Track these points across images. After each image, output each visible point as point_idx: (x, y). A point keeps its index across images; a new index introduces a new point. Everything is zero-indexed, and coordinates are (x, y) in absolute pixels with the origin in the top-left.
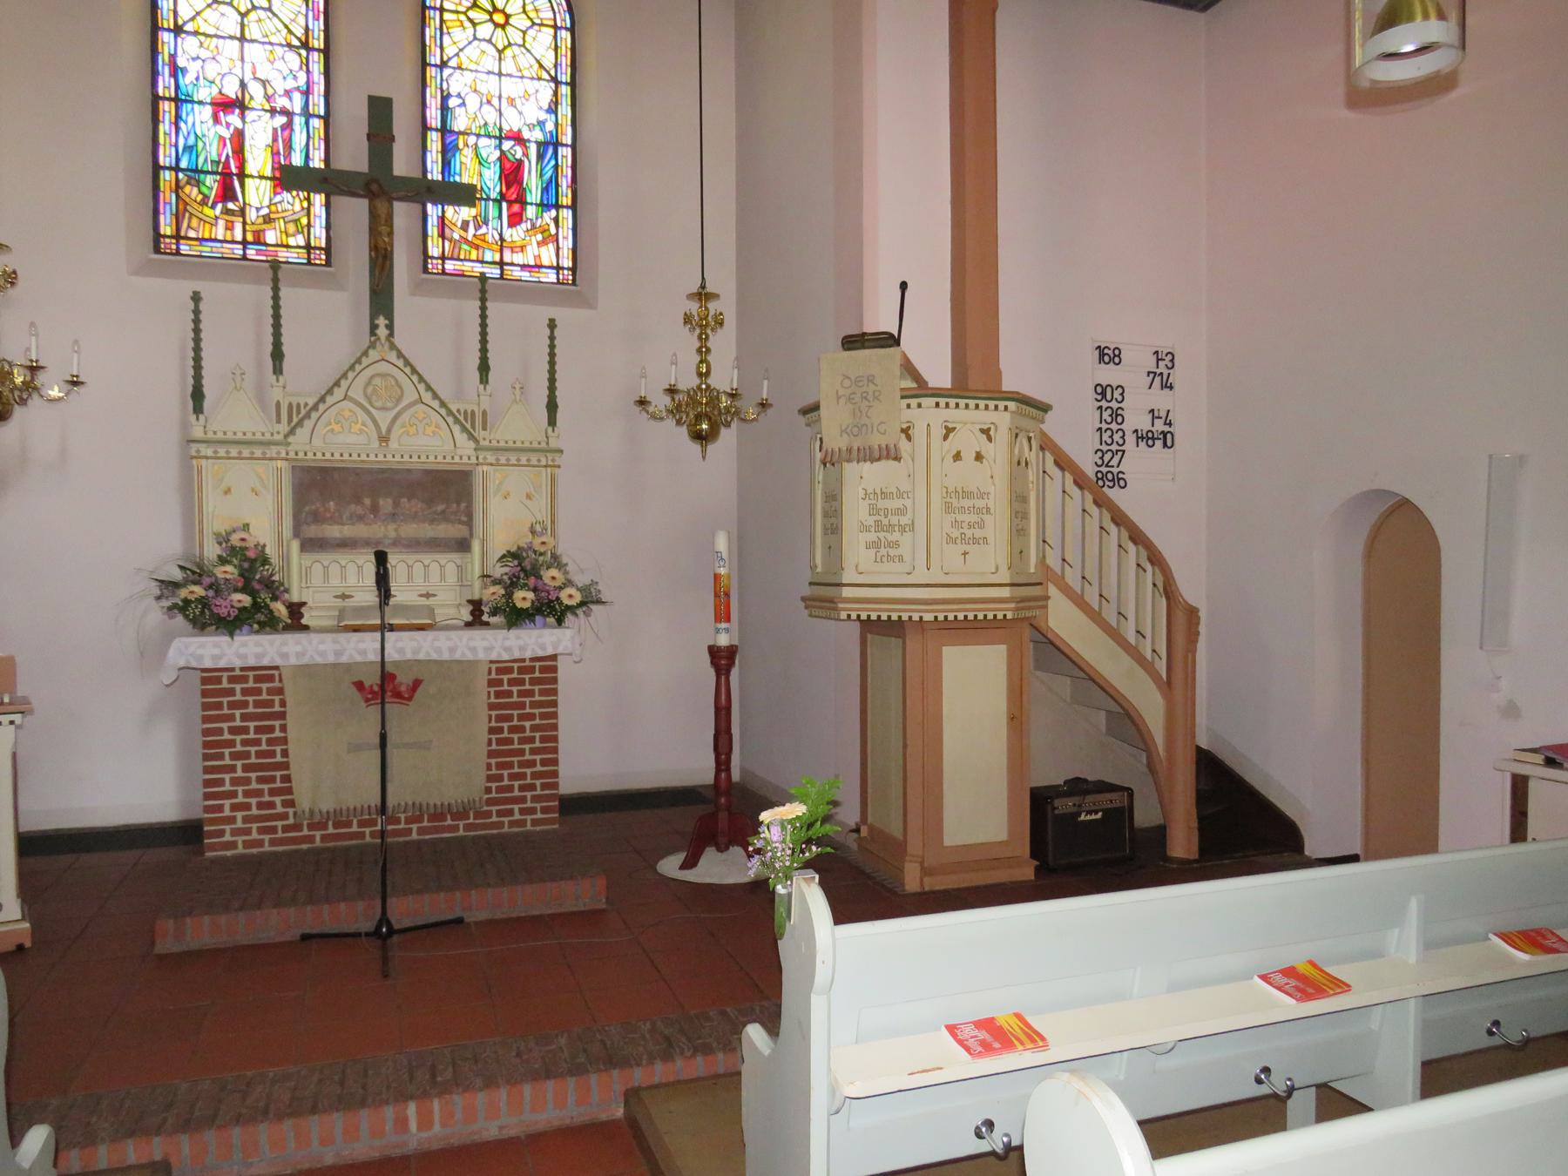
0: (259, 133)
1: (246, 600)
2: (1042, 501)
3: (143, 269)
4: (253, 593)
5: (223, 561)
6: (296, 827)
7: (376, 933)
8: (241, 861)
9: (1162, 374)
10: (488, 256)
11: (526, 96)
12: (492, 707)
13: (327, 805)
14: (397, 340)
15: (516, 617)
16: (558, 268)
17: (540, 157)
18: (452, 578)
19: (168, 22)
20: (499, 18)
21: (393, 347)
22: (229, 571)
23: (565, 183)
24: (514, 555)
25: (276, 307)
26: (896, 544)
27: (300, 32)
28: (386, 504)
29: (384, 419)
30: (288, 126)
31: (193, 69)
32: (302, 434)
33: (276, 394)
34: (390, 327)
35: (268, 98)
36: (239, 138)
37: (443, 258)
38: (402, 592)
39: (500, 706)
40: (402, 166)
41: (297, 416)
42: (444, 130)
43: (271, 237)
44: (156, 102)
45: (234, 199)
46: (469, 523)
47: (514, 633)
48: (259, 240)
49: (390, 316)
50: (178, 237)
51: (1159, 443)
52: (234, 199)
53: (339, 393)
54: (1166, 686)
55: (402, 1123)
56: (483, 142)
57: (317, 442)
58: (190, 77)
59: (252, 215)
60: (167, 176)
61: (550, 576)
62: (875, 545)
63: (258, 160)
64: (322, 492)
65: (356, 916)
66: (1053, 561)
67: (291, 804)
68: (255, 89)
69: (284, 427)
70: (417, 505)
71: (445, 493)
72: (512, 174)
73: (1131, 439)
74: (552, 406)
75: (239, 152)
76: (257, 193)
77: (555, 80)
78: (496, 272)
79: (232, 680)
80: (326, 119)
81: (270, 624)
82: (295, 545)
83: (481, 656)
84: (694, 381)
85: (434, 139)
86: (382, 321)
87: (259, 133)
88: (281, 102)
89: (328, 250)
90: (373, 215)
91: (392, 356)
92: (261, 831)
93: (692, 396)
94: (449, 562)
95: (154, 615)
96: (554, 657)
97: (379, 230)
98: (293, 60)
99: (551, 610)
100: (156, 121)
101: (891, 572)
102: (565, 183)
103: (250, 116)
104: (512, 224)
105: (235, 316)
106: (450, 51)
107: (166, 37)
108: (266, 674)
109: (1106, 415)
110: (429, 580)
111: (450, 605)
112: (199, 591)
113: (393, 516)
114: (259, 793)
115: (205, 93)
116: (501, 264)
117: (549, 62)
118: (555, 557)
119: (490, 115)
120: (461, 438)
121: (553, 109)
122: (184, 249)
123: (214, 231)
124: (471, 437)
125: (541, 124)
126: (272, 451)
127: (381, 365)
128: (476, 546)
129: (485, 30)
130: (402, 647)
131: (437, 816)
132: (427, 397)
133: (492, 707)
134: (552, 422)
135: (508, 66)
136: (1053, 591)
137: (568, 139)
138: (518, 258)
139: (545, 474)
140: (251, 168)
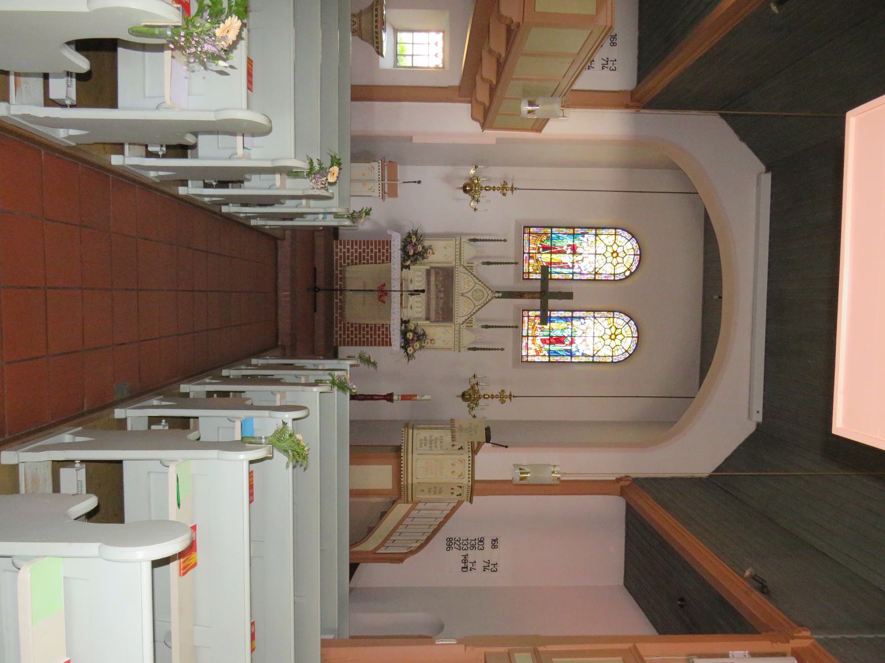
0: (566, 258)
1: (411, 253)
2: (439, 501)
3: (517, 223)
4: (413, 255)
5: (423, 247)
6: (341, 266)
7: (315, 287)
8: (332, 251)
9: (490, 567)
10: (530, 332)
11: (587, 345)
12: (375, 325)
13: (347, 275)
14: (494, 300)
15: (404, 334)
16: (527, 356)
17: (566, 350)
18: (416, 315)
19: (598, 232)
20: (613, 337)
21: (492, 298)
22: (420, 248)
23: (558, 359)
24: (424, 334)
25: (509, 263)
26: (425, 445)
27: (600, 272)
28: (442, 295)
29: (469, 295)
30: (569, 267)
31: (585, 239)
32: (463, 270)
33: (476, 263)
34: (499, 297)
35: (577, 262)
36: (564, 252)
37: (528, 316)
38: (413, 300)
39: (375, 328)
40: (552, 303)
41: (469, 269)
42: (572, 318)
43: (531, 261)
44: (575, 229)
45: (543, 250)
46: (435, 321)
47: (399, 332)
48: (530, 257)
49: (502, 297)
50: (530, 233)
51: (463, 565)
52: (543, 250)
53: (477, 281)
54: (374, 552)
55: (286, 291)
56: (570, 331)
57: (461, 274)
58: (581, 238)
59: (538, 256)
60: (549, 230)
61: (417, 345)
62: (425, 439)
63: (556, 258)
64: (445, 277)
65: (320, 283)
66: (420, 506)
67: (348, 265)
68: (580, 258)
69: (465, 265)
70: (441, 305)
71: (446, 314)
72: (559, 340)
73: (464, 553)
74: (475, 349)
75: (559, 252)
76: (545, 258)
77: (594, 356)
78: (525, 334)
79: (387, 250)
80: (572, 279)
81: (404, 260)
82: (428, 267)
83: (392, 322)
84: (482, 393)
85: (569, 314)
86: (500, 295)
87: (566, 258)
88: (576, 265)
89: (528, 279)
90: (534, 293)
91: (489, 298)
92: (341, 257)
93: (475, 392)
94: (423, 314)
95: (408, 229)
96: (391, 345)
97: (531, 295)
98: (591, 270)
99: (406, 344)
100: (567, 228)
101: (417, 444)
102: (558, 359)
103: (571, 256)
104: (542, 340)
105: (507, 251)
106: (600, 320)
107: (594, 232)
108: (389, 259)
109: (473, 542)
110: (416, 308)
111: (408, 314)
112: (414, 241)
113: (437, 297)
114: (352, 255)
115: (577, 242)
116: (528, 336)
117: (599, 354)
118: (423, 347)
119: (579, 333)
120: (464, 319)
121: (583, 355)
122: (526, 235)
123: (532, 245)
124: (464, 322)
125: (578, 351)
126: (458, 261)
127: (488, 294)
128: (428, 322)
129: (608, 332)
130: (395, 297)
131: (342, 308)
132: (477, 308)
133: (375, 325)
134: (469, 349)
135: (597, 339)
136: (410, 505)
137: (574, 360)
138: (530, 342)
139: (451, 345)
140: (554, 256)
